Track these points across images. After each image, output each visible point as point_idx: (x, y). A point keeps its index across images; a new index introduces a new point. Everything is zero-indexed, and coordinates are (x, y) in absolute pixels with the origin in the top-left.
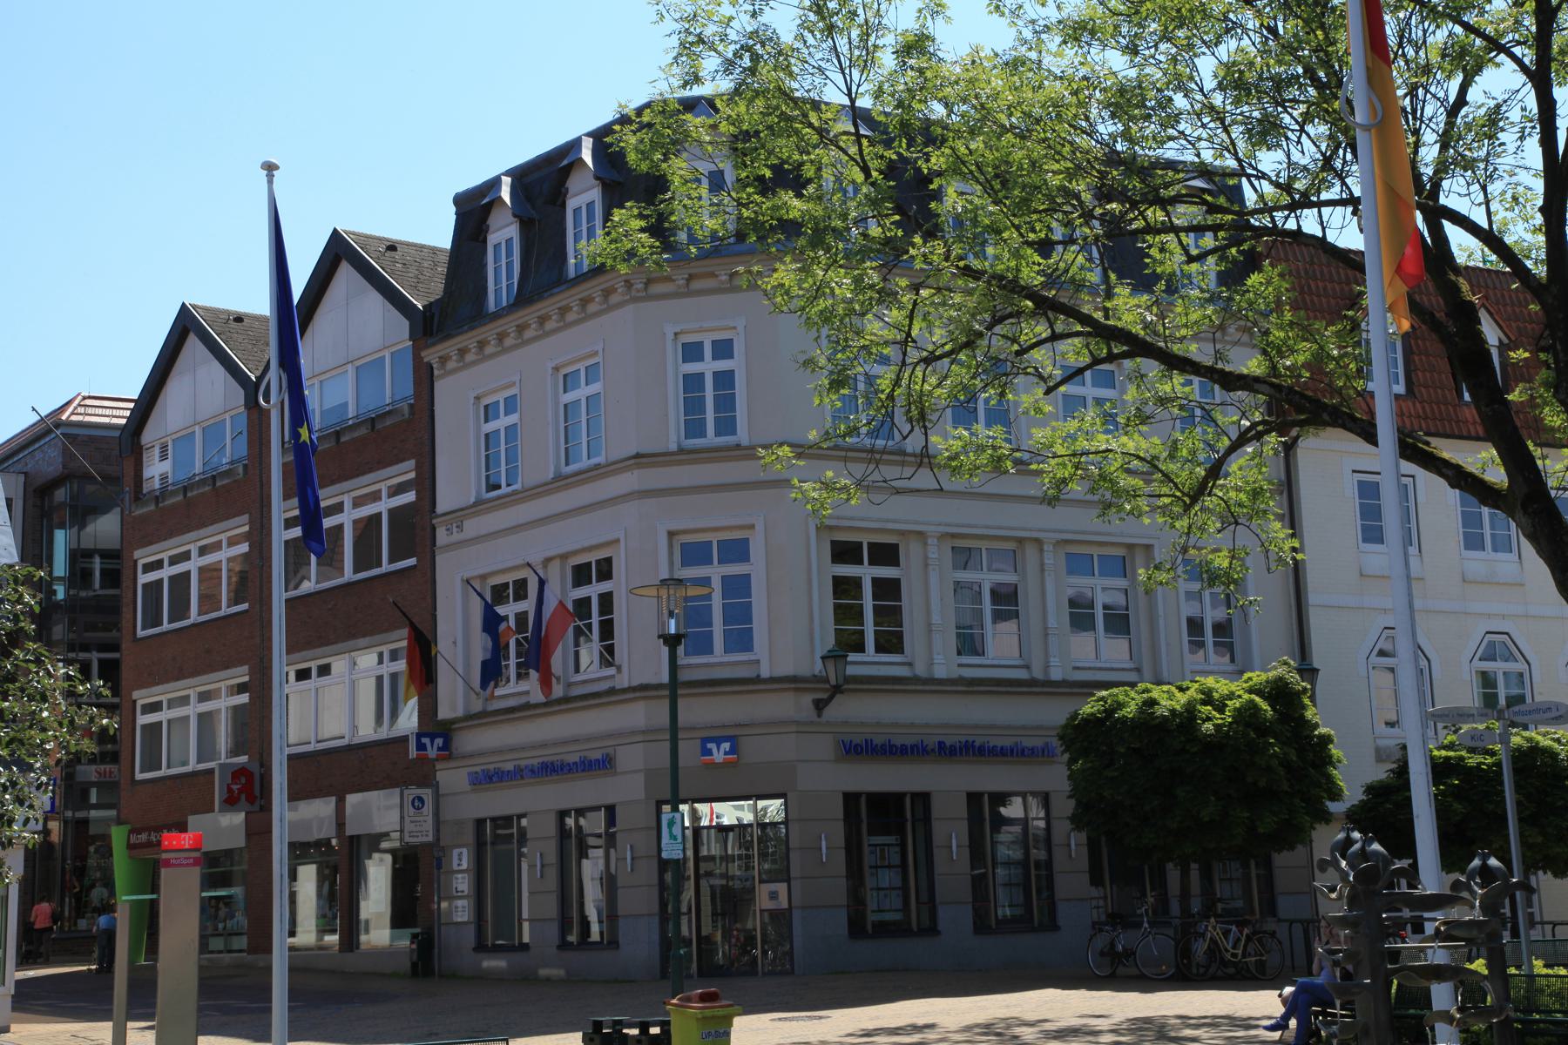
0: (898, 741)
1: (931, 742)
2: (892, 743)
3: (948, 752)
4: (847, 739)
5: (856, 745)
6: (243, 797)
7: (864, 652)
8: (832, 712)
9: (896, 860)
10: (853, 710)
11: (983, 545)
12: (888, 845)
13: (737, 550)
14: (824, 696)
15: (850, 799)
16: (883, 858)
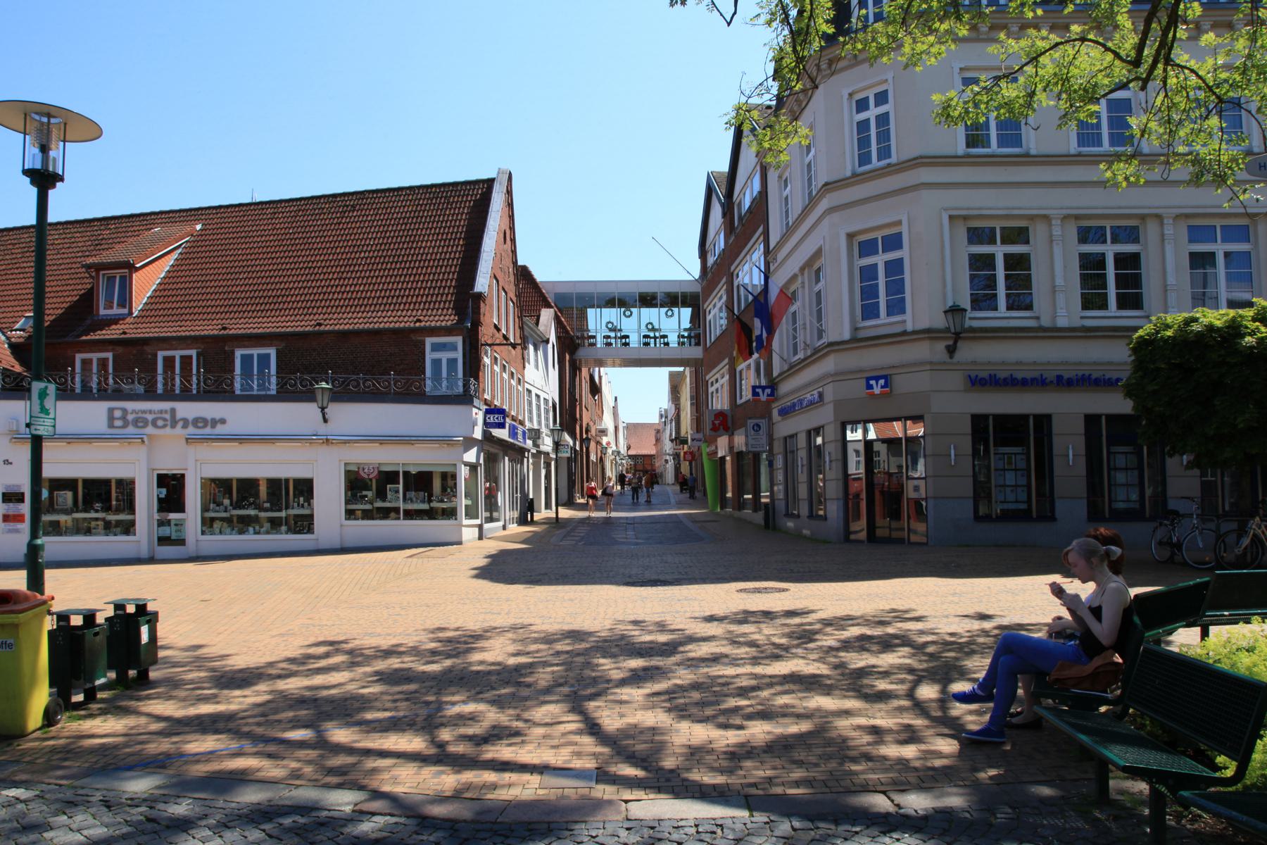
0: (1020, 376)
1: (1050, 376)
2: (1014, 376)
3: (1065, 383)
4: (973, 375)
5: (981, 379)
6: (721, 427)
7: (1107, 309)
8: (960, 356)
9: (1022, 465)
10: (972, 352)
11: (1218, 223)
12: (1015, 454)
13: (894, 242)
14: (951, 342)
15: (978, 421)
16: (1010, 463)
